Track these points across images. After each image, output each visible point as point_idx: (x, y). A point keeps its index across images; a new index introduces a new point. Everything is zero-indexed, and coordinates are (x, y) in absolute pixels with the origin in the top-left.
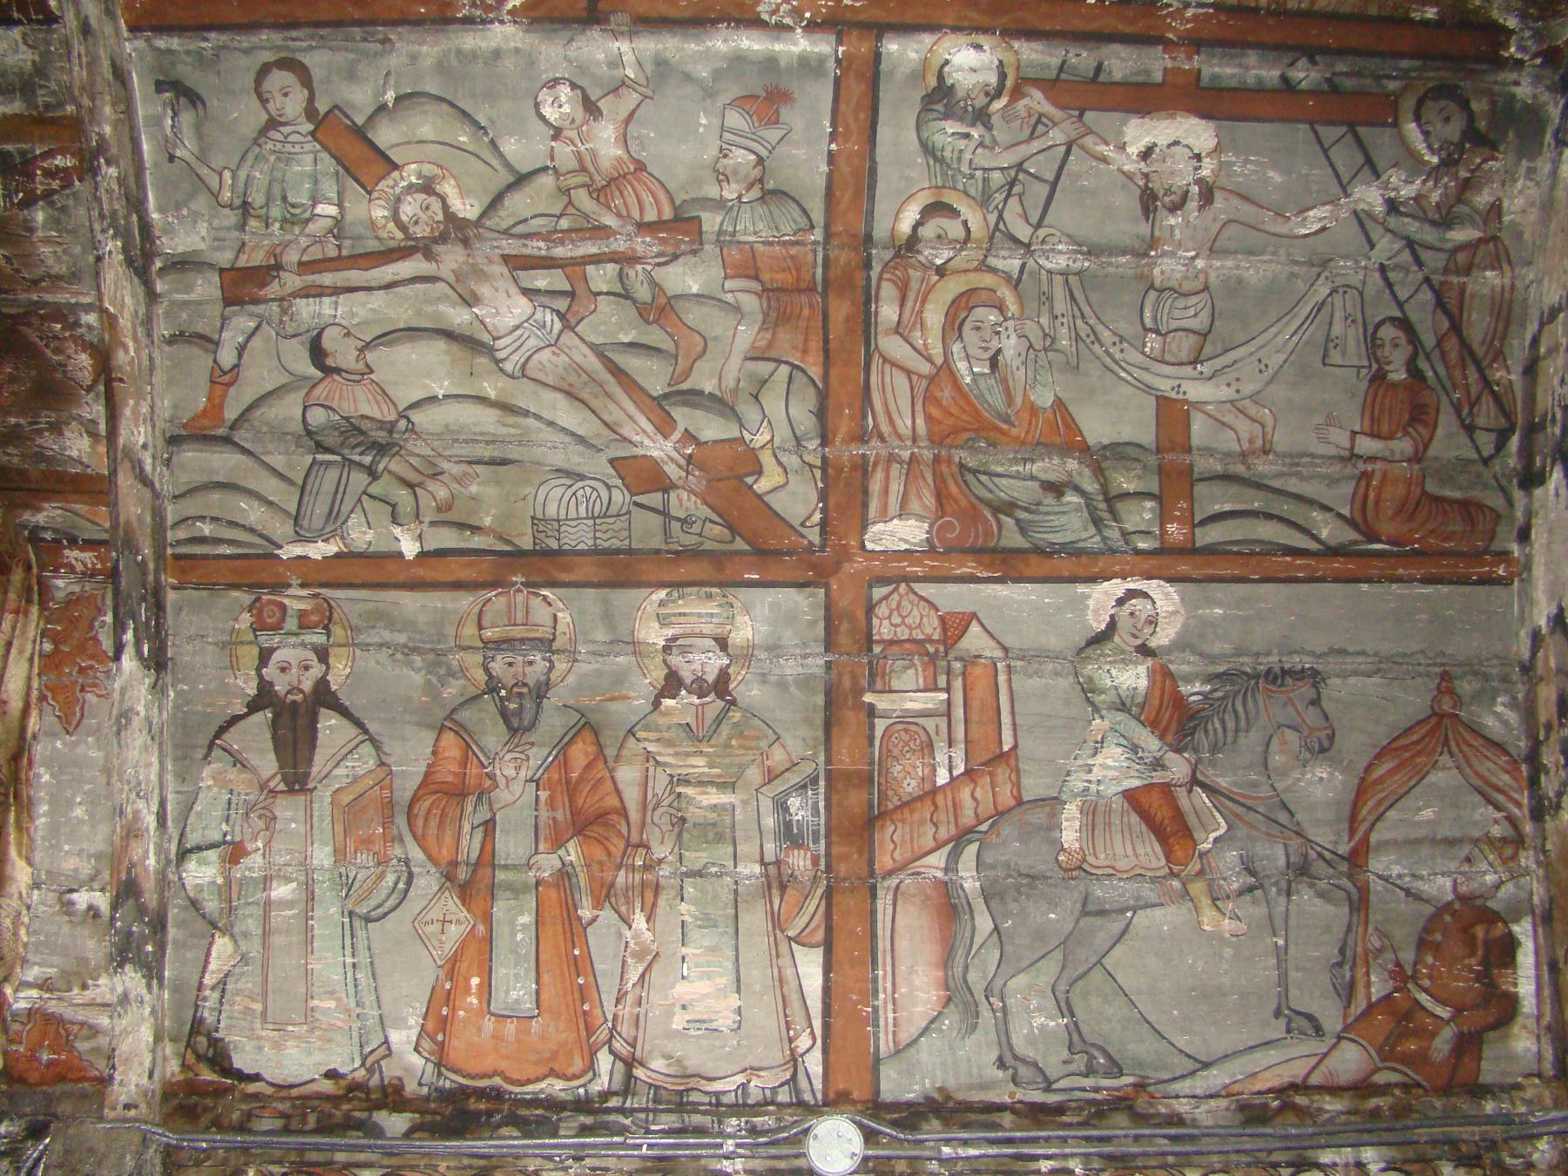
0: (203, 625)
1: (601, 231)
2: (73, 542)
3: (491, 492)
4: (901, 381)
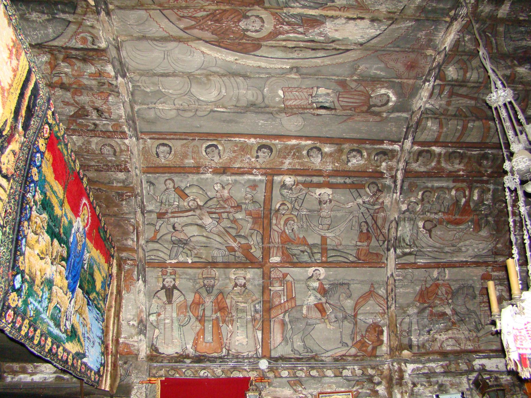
0: (153, 274)
1: (225, 208)
2: (129, 259)
3: (204, 252)
4: (276, 233)
